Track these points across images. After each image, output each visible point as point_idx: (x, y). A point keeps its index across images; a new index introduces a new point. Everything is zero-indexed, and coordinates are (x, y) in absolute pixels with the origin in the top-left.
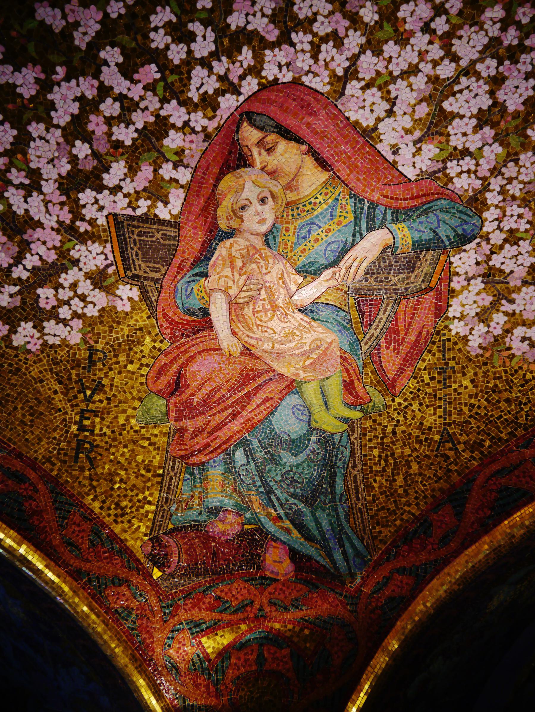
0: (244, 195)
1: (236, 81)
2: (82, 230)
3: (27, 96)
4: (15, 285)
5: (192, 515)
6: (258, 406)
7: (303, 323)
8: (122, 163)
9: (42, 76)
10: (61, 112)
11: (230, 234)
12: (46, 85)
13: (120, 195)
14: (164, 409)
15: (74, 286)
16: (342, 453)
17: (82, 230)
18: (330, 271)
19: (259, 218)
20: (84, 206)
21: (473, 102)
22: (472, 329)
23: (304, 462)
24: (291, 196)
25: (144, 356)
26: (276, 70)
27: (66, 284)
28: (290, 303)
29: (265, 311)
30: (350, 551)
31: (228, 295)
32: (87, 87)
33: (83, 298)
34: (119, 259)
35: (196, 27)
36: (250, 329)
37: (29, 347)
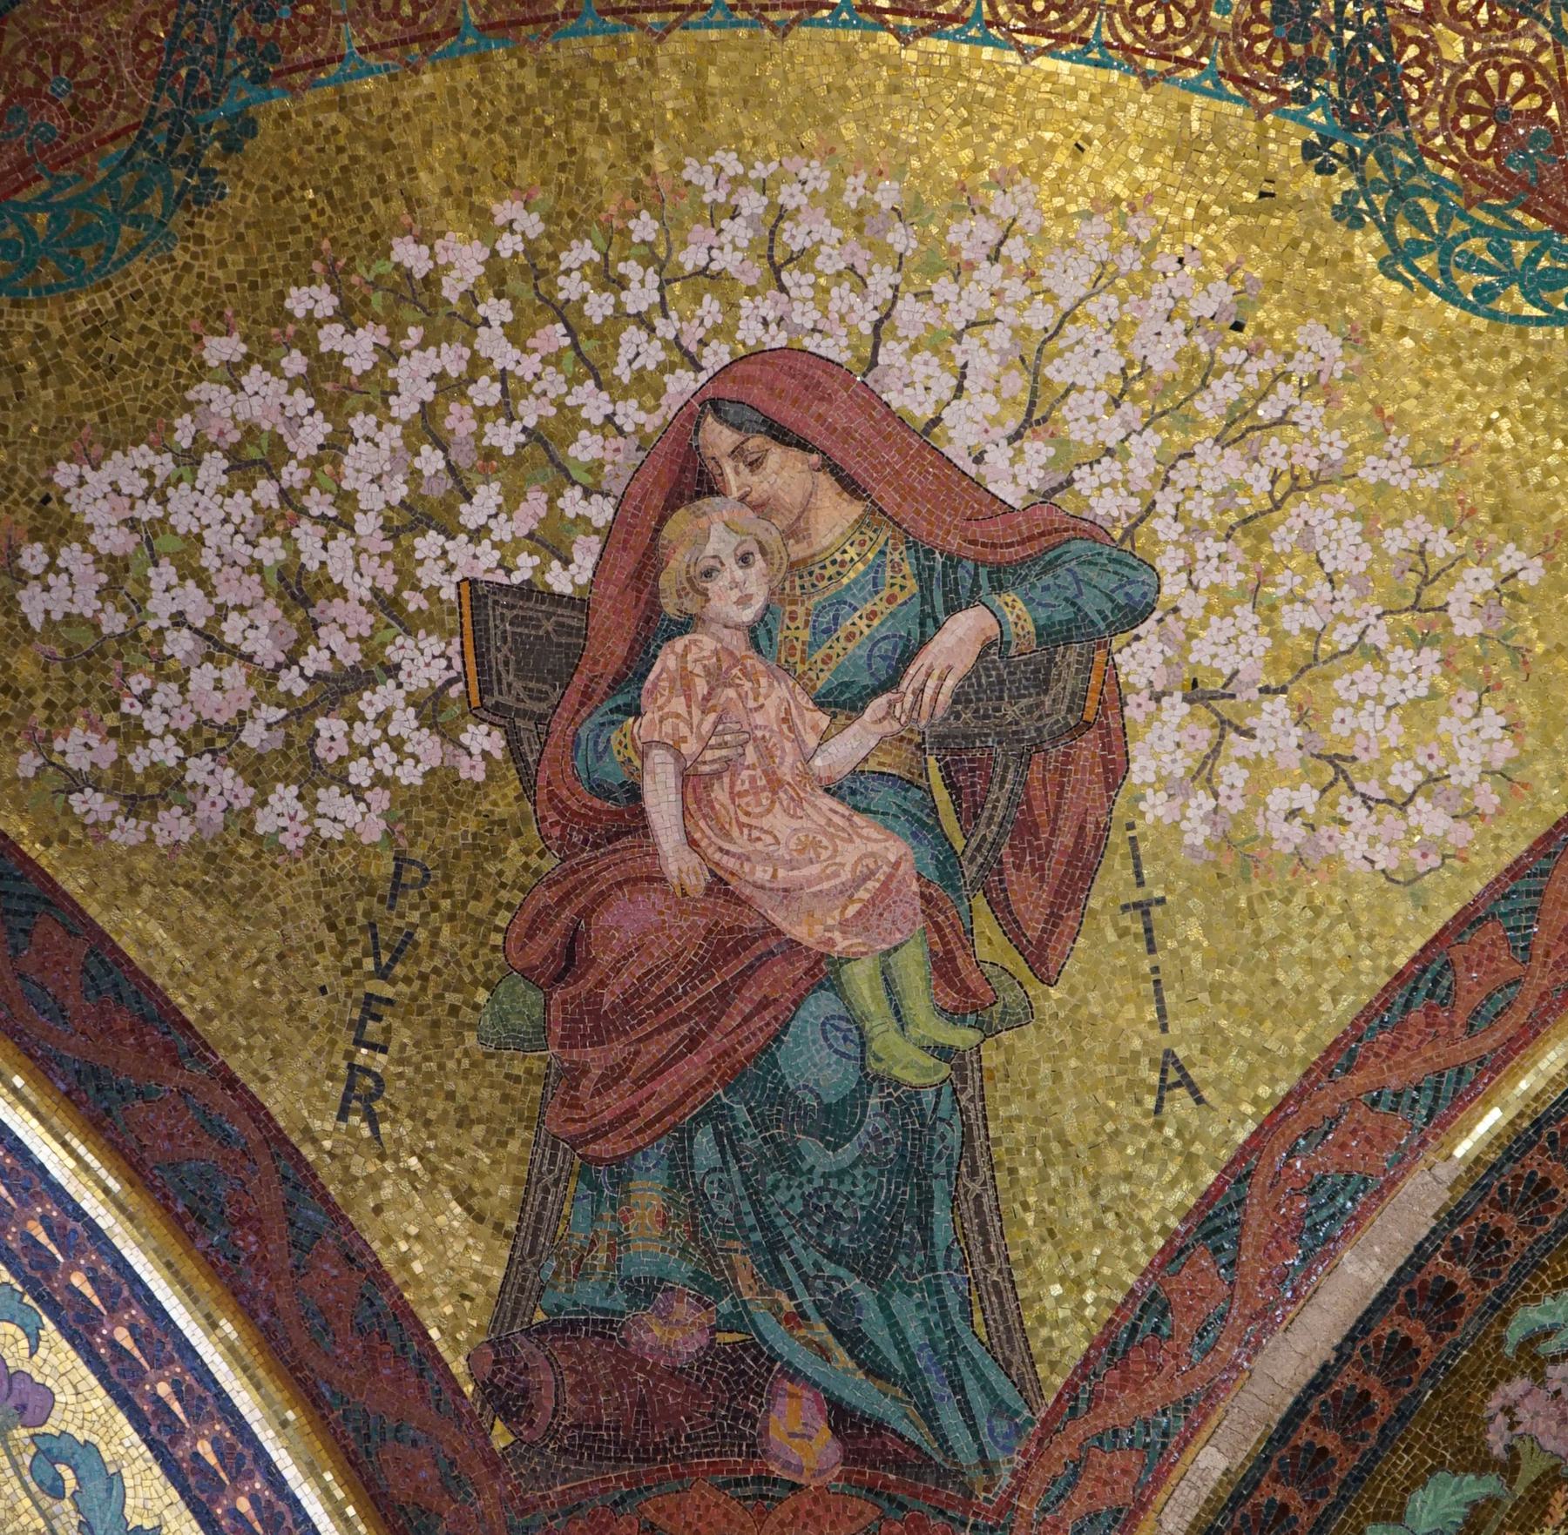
0: (710, 550)
1: (693, 348)
2: (412, 607)
3: (357, 371)
4: (279, 706)
5: (589, 1293)
6: (747, 1019)
7: (836, 819)
8: (495, 486)
9: (386, 342)
10: (405, 396)
11: (686, 624)
12: (389, 355)
13: (486, 543)
14: (537, 1013)
15: (384, 718)
16: (943, 1138)
17: (412, 607)
18: (882, 701)
19: (738, 595)
20: (421, 562)
21: (1094, 362)
22: (1185, 806)
23: (854, 1165)
24: (798, 551)
25: (503, 886)
26: (759, 329)
27: (370, 714)
28: (806, 775)
29: (755, 790)
30: (979, 1402)
31: (678, 756)
32: (452, 360)
33: (397, 745)
34: (472, 668)
35: (630, 269)
36: (727, 836)
37: (282, 838)
